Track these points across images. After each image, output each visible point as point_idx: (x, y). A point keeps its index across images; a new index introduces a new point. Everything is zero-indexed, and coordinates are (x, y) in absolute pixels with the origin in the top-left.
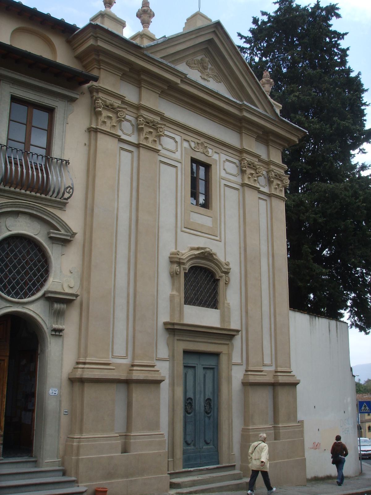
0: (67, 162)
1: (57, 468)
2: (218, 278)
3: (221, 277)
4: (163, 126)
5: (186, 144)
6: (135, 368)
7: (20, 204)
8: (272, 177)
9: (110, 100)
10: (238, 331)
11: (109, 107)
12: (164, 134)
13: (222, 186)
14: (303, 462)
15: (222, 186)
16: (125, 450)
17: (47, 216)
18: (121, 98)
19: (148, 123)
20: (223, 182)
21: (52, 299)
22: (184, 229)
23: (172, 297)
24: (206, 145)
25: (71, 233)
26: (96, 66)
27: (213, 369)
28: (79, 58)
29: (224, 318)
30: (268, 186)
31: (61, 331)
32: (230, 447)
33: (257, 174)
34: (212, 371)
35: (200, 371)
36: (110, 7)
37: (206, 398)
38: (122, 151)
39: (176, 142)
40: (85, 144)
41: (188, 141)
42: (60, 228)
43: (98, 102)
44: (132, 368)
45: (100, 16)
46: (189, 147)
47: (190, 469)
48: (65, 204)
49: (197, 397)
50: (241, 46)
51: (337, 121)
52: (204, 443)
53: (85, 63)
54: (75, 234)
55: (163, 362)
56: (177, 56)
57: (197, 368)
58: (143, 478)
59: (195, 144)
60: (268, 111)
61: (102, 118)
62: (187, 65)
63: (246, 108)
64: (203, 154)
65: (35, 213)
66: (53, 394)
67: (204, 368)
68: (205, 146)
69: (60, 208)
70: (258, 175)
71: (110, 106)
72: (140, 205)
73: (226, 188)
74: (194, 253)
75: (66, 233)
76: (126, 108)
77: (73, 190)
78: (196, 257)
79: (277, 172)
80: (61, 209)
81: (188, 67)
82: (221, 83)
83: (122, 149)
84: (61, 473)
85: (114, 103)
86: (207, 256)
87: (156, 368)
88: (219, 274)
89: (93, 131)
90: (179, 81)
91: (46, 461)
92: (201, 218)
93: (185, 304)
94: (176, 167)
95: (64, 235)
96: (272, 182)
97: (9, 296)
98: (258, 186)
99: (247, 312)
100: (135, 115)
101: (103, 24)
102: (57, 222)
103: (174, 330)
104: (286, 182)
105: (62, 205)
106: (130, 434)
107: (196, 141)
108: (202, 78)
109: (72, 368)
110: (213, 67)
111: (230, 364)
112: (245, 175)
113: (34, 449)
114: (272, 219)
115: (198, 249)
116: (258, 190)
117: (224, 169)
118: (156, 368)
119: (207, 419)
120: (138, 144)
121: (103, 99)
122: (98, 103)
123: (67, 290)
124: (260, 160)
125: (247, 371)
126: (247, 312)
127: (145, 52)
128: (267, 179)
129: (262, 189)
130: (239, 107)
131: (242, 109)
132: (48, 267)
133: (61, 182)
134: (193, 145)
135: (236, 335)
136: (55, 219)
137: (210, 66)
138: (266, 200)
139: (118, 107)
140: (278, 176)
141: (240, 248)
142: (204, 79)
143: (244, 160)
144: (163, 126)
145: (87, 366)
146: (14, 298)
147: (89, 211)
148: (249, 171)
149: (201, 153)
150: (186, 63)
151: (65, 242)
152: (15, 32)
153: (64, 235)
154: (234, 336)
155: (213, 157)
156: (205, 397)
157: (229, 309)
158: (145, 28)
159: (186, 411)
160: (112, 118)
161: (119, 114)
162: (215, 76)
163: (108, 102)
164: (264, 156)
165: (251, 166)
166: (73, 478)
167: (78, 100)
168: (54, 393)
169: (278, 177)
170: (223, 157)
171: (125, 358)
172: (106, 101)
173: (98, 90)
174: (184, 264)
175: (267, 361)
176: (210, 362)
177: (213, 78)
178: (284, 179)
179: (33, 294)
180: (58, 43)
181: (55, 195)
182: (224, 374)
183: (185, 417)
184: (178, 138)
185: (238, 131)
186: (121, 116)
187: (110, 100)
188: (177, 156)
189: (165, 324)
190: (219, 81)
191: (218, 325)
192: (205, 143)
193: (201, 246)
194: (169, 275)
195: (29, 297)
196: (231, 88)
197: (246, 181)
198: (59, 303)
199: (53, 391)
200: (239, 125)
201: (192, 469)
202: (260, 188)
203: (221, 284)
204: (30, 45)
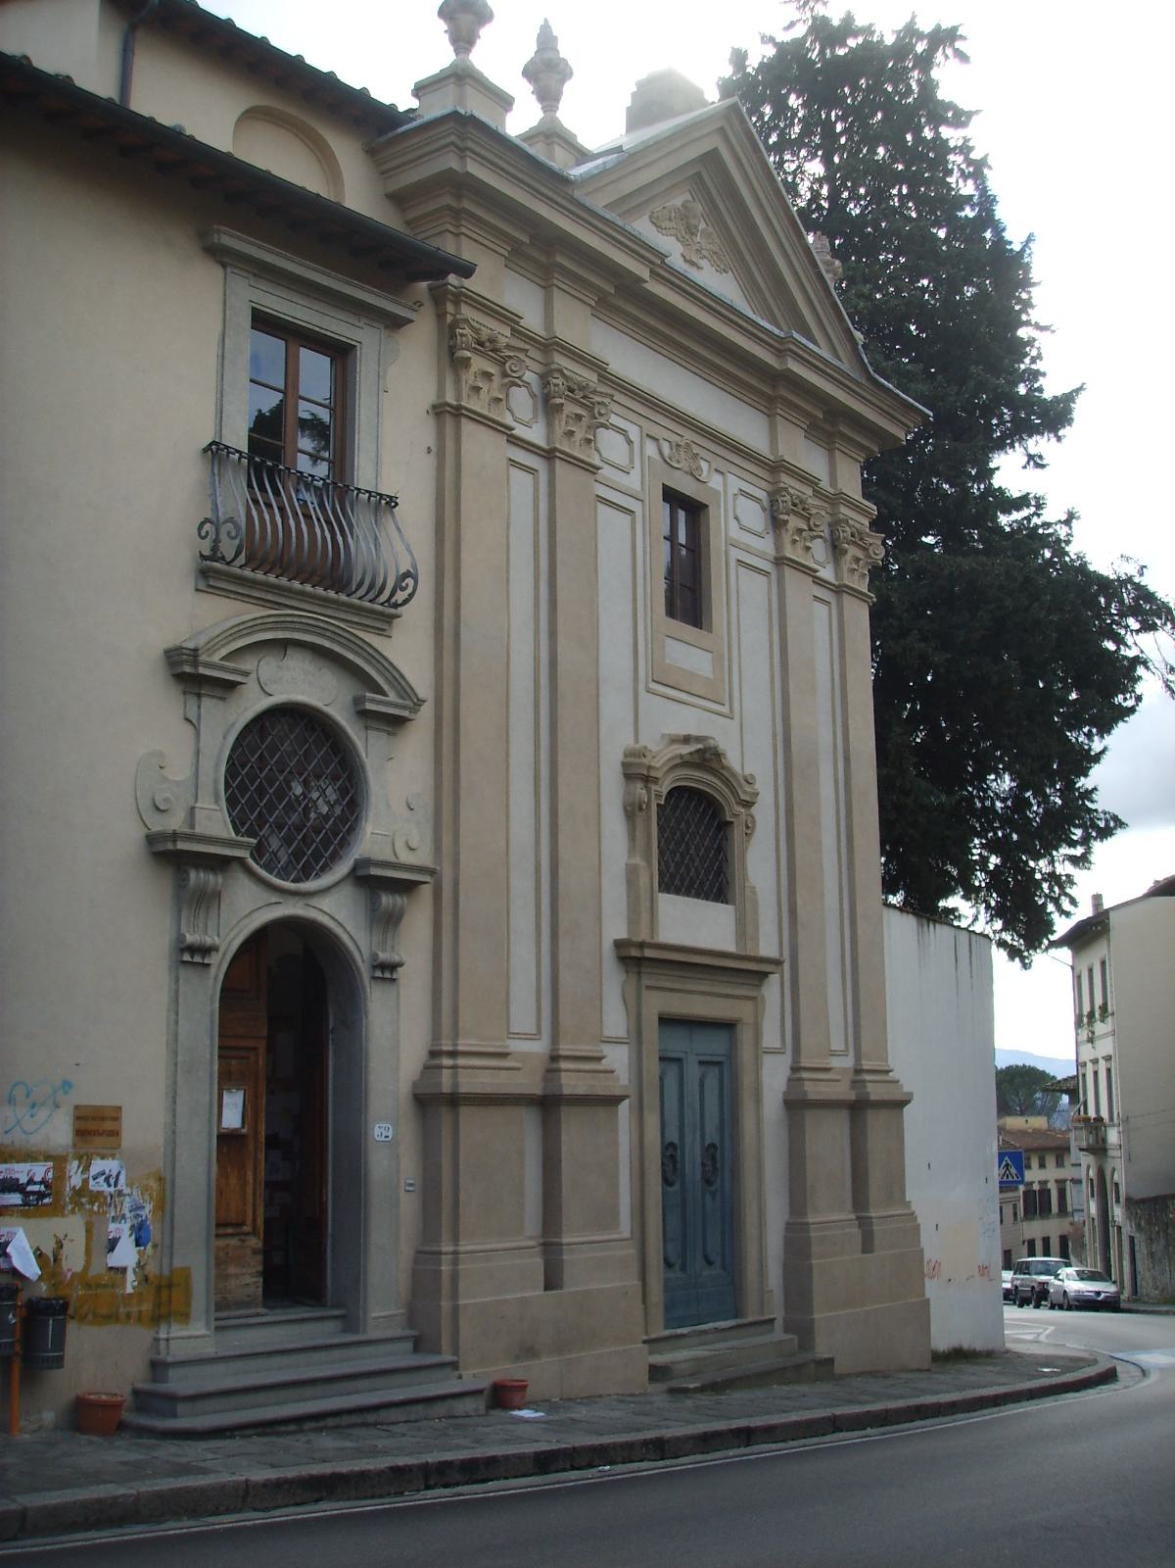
0: (392, 502)
1: (400, 1332)
2: (728, 819)
3: (736, 816)
4: (607, 400)
5: (651, 449)
6: (564, 1065)
7: (295, 619)
8: (844, 538)
9: (491, 327)
10: (778, 963)
11: (487, 346)
12: (523, 381)
13: (733, 564)
14: (922, 1310)
15: (733, 564)
16: (552, 1282)
17: (356, 653)
18: (509, 318)
19: (572, 391)
20: (735, 554)
21: (370, 882)
22: (653, 686)
23: (632, 873)
24: (696, 450)
25: (413, 701)
26: (448, 220)
27: (719, 1064)
28: (399, 199)
29: (744, 928)
30: (832, 563)
31: (393, 967)
32: (762, 1273)
33: (810, 530)
34: (716, 1070)
35: (693, 1071)
36: (468, 51)
37: (707, 1143)
38: (512, 469)
39: (630, 442)
40: (429, 450)
41: (657, 440)
42: (386, 687)
43: (464, 331)
44: (554, 1066)
45: (452, 80)
46: (657, 457)
47: (679, 1331)
48: (390, 619)
49: (688, 1139)
50: (1073, 405)
51: (979, 375)
52: (704, 1262)
53: (412, 214)
54: (420, 703)
55: (614, 1043)
56: (632, 203)
57: (685, 1061)
58: (593, 1353)
59: (671, 449)
60: (841, 353)
61: (469, 378)
62: (653, 223)
63: (795, 349)
64: (689, 477)
65: (327, 644)
66: (383, 1139)
67: (701, 1063)
68: (695, 452)
69: (378, 629)
70: (815, 534)
71: (488, 344)
72: (560, 620)
73: (742, 570)
74: (678, 752)
75: (401, 701)
76: (527, 351)
77: (416, 582)
78: (685, 763)
79: (857, 525)
80: (380, 632)
81: (654, 228)
82: (727, 272)
83: (513, 463)
84: (409, 1345)
85: (500, 336)
86: (707, 758)
87: (605, 1064)
88: (732, 810)
89: (447, 414)
90: (644, 272)
91: (374, 1315)
92: (687, 653)
93: (659, 891)
94: (631, 512)
95: (396, 706)
96: (845, 552)
97: (287, 880)
98: (508, 420)
99: (793, 912)
100: (769, 488)
101: (550, 160)
102: (378, 670)
103: (638, 959)
104: (877, 552)
105: (384, 620)
106: (557, 1240)
107: (675, 438)
108: (686, 261)
109: (420, 1067)
110: (711, 229)
111: (759, 1052)
112: (783, 532)
113: (329, 1283)
114: (842, 656)
115: (687, 740)
116: (507, 435)
117: (736, 518)
118: (605, 1064)
119: (708, 1198)
120: (550, 449)
121: (475, 324)
122: (462, 335)
123: (405, 857)
124: (818, 493)
125: (795, 1069)
126: (793, 912)
127: (577, 194)
128: (828, 543)
129: (520, 431)
130: (777, 345)
131: (785, 350)
132: (355, 793)
133: (378, 558)
134: (666, 451)
135: (771, 973)
136: (374, 662)
137: (702, 226)
138: (828, 603)
139: (508, 347)
140: (856, 535)
141: (774, 736)
142: (692, 263)
143: (783, 494)
144: (607, 400)
145: (461, 1061)
146: (283, 880)
147: (446, 637)
148: (794, 522)
149: (686, 472)
150: (650, 217)
151: (395, 723)
152: (251, 115)
153: (396, 706)
154: (765, 975)
155: (710, 485)
156: (703, 1138)
157: (755, 902)
158: (461, 56)
159: (667, 1181)
160: (493, 378)
161: (507, 365)
162: (715, 253)
163: (485, 334)
164: (533, 321)
165: (799, 508)
166: (448, 1357)
167: (411, 324)
168: (384, 1134)
169: (857, 539)
170: (735, 484)
171: (536, 1036)
172: (480, 329)
173: (459, 297)
174: (656, 780)
175: (837, 1044)
176: (713, 1045)
177: (709, 261)
178: (870, 544)
179: (325, 868)
180: (346, 151)
181: (371, 596)
182: (747, 1080)
183: (664, 1193)
184: (634, 433)
185: (765, 410)
186: (876, 554)
187: (491, 327)
188: (633, 481)
189: (619, 944)
190: (723, 267)
191: (731, 948)
192: (694, 445)
193: (693, 732)
194: (622, 812)
195: (317, 876)
196: (750, 287)
197: (789, 553)
198: (380, 886)
199: (382, 1130)
200: (543, 259)
201: (684, 1331)
202: (818, 571)
203: (737, 833)
204: (283, 160)
